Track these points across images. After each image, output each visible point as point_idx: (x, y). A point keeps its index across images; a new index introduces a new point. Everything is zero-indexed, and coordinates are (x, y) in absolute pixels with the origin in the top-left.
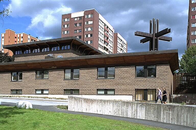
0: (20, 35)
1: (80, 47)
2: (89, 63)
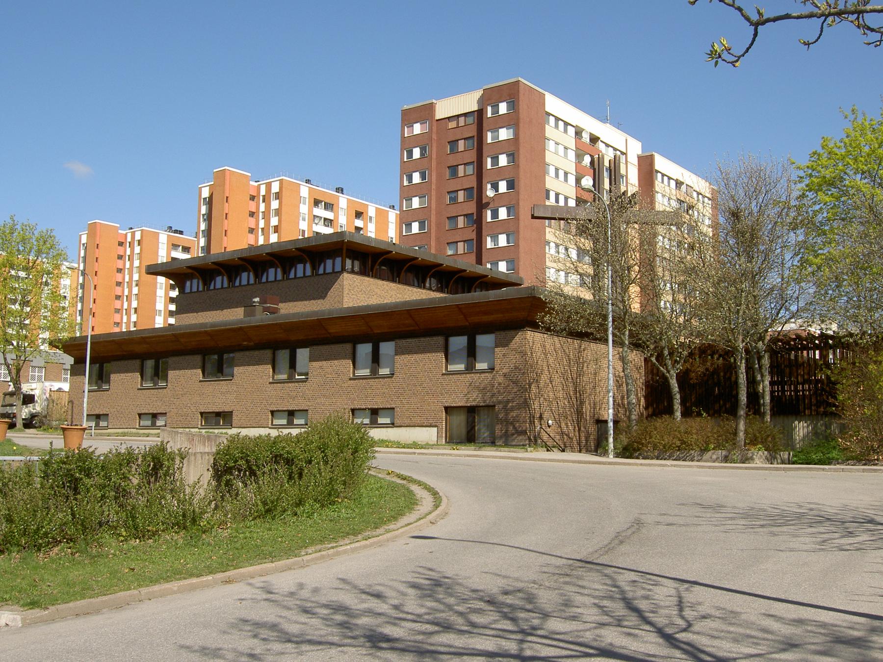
0: (269, 186)
1: (384, 258)
2: (334, 330)
